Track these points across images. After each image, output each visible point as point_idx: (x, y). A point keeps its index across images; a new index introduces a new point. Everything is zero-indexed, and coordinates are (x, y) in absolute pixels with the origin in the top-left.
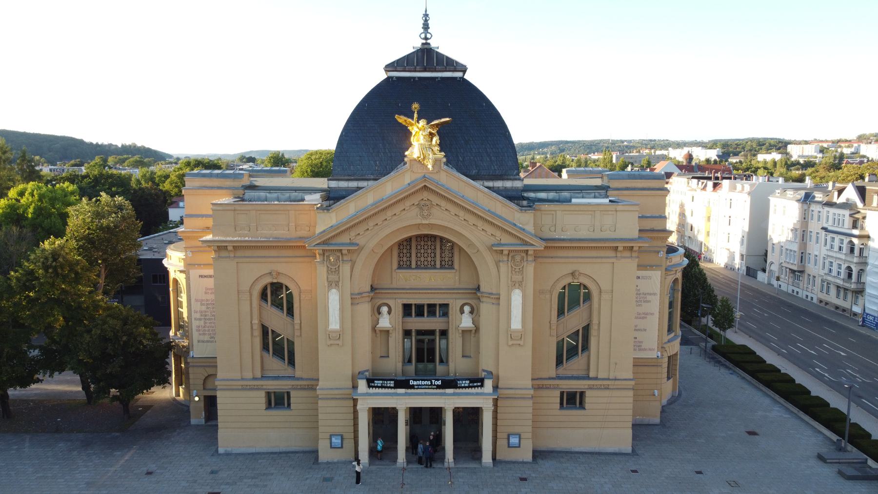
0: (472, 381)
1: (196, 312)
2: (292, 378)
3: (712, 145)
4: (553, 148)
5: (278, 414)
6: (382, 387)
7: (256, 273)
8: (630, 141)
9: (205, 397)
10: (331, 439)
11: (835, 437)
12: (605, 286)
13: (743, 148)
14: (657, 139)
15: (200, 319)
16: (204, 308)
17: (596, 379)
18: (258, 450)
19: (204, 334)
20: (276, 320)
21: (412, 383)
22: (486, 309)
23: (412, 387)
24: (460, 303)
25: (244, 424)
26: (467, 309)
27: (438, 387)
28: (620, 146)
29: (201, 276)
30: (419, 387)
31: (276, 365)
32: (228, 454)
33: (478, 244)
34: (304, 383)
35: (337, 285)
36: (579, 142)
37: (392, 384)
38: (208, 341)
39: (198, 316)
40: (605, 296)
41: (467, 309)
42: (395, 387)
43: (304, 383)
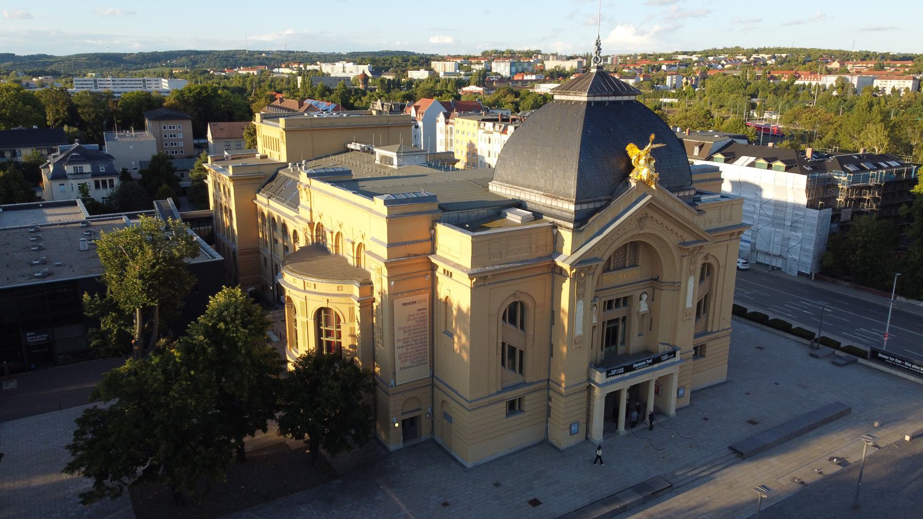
0: (669, 354)
1: (399, 340)
2: (524, 384)
3: (356, 58)
4: (184, 59)
5: (516, 418)
6: (616, 374)
7: (502, 297)
8: (267, 53)
9: (403, 421)
10: (570, 428)
11: (809, 343)
12: (722, 263)
13: (391, 63)
14: (295, 50)
15: (402, 347)
16: (406, 335)
17: (719, 331)
18: (499, 455)
19: (406, 361)
20: (514, 337)
21: (635, 366)
22: (665, 296)
23: (635, 369)
24: (638, 293)
25: (480, 434)
26: (645, 297)
27: (650, 364)
28: (259, 58)
29: (404, 304)
30: (639, 368)
31: (513, 377)
32: (477, 467)
33: (669, 243)
34: (536, 386)
35: (583, 297)
36: (211, 52)
37: (622, 370)
38: (409, 367)
39: (401, 344)
40: (721, 270)
41: (645, 297)
42: (625, 372)
43: (536, 386)
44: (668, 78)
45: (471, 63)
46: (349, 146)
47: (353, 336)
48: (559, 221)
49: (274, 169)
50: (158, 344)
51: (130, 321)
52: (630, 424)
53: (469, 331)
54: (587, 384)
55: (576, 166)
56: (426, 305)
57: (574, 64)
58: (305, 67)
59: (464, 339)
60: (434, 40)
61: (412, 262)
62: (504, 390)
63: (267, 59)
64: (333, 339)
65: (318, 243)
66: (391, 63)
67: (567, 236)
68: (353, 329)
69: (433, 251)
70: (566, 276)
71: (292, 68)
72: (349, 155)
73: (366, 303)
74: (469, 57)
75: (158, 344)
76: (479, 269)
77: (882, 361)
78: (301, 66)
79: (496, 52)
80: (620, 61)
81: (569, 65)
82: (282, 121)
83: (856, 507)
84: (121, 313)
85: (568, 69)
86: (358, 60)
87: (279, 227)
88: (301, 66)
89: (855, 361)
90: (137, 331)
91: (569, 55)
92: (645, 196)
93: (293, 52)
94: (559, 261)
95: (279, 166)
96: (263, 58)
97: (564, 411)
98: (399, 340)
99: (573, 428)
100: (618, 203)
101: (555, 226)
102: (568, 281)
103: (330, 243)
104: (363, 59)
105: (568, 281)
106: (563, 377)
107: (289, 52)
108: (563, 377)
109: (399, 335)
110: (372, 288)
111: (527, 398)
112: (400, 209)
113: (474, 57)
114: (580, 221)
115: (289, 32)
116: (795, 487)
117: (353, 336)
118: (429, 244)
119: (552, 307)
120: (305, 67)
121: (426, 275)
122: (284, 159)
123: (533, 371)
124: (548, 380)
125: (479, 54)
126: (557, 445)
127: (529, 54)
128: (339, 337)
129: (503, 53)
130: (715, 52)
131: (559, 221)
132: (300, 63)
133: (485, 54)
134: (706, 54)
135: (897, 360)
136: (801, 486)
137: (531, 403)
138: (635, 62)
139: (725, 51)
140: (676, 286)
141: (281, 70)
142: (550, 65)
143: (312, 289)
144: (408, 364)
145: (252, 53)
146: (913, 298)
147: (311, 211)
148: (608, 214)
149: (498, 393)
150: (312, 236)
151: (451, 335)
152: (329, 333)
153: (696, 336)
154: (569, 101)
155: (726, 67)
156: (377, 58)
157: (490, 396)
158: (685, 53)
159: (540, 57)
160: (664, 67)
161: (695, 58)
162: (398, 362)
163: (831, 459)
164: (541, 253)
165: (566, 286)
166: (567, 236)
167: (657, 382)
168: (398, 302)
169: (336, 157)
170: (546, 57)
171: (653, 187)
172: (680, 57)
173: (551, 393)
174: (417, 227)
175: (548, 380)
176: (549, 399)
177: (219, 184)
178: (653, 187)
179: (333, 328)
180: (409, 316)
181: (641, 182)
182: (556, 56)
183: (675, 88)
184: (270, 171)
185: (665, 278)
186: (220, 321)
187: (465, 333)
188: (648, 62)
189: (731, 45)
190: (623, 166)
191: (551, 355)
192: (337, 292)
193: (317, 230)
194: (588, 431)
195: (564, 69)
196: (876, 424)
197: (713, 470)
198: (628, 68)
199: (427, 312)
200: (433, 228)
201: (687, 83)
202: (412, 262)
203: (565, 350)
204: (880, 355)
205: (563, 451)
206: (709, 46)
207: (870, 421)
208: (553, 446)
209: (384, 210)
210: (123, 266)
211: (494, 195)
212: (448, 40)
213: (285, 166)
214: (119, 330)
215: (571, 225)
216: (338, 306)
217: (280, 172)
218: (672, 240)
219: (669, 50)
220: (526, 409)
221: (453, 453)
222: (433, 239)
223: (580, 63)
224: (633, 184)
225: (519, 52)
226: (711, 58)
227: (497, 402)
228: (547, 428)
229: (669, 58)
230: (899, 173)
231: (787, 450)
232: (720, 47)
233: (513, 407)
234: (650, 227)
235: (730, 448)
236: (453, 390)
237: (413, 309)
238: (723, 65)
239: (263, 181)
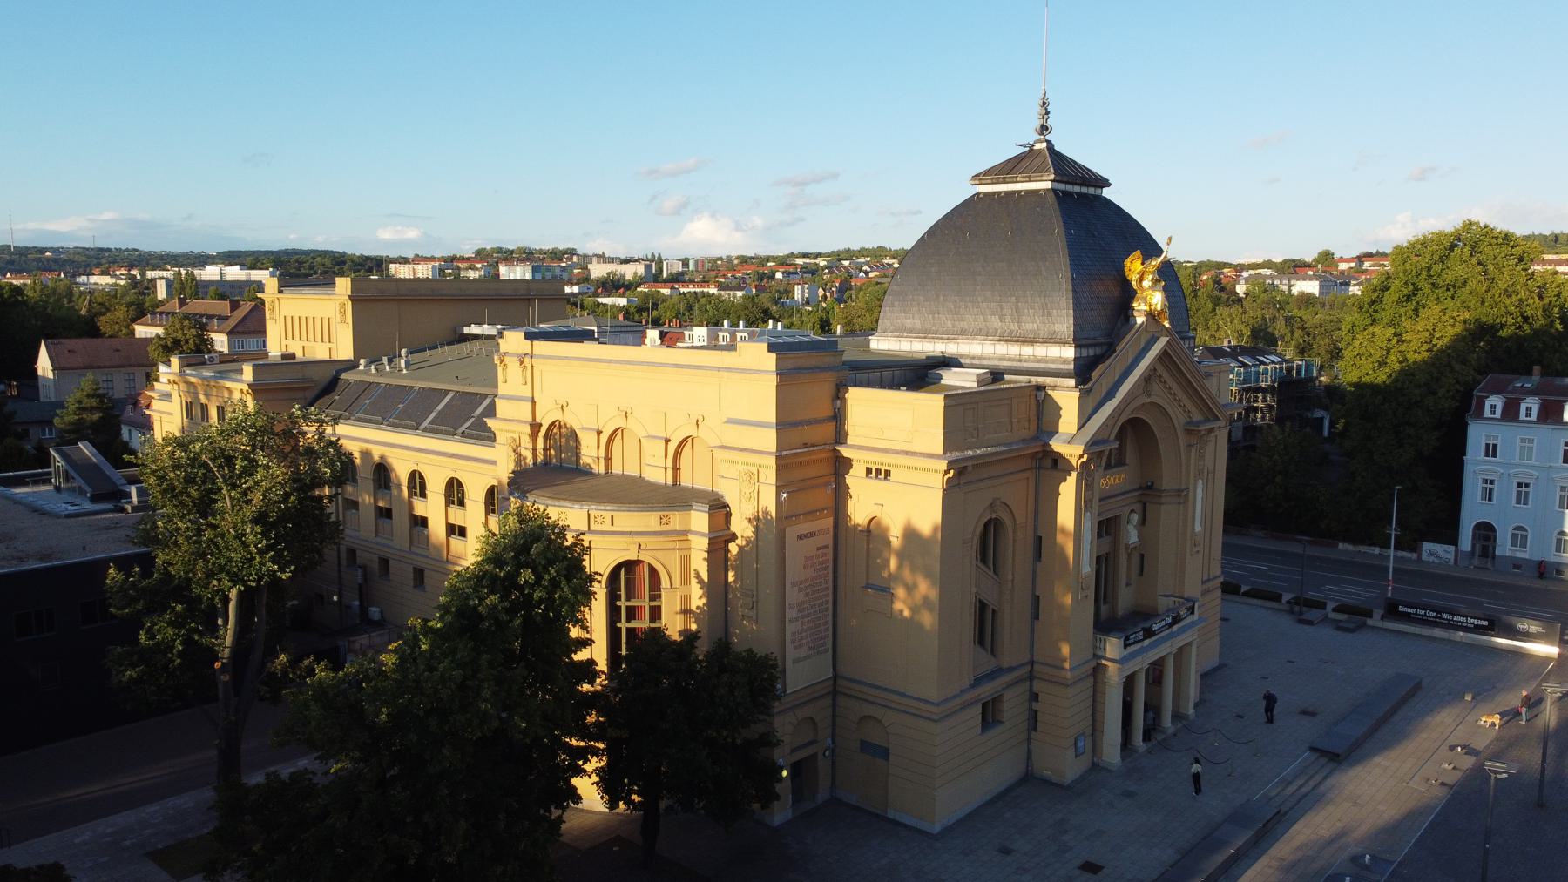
8: (54, 250)
15: (796, 619)
22: (1166, 513)
24: (1127, 510)
25: (947, 771)
27: (1171, 625)
29: (800, 537)
34: (1016, 674)
38: (805, 658)
43: (1016, 674)
44: (798, 289)
45: (459, 269)
46: (466, 330)
47: (686, 612)
48: (1041, 380)
49: (331, 373)
50: (271, 668)
51: (210, 617)
52: (1147, 736)
53: (937, 567)
54: (1093, 664)
55: (1066, 285)
56: (828, 539)
57: (640, 269)
58: (143, 274)
59: (924, 587)
60: (386, 234)
61: (813, 458)
62: (978, 682)
63: (56, 261)
64: (643, 624)
65: (546, 463)
66: (311, 267)
67: (1067, 399)
68: (686, 598)
69: (840, 437)
70: (1068, 469)
71: (115, 276)
72: (466, 347)
73: (720, 540)
74: (453, 259)
75: (271, 668)
76: (957, 455)
77: (1406, 617)
78: (134, 272)
79: (499, 250)
80: (707, 266)
81: (630, 272)
82: (343, 285)
83: (1540, 805)
84: (192, 603)
85: (629, 277)
86: (248, 260)
87: (365, 474)
88: (134, 272)
89: (1364, 625)
90: (228, 641)
91: (623, 257)
92: (1154, 340)
93: (109, 250)
94: (1057, 445)
95: (338, 367)
96: (48, 259)
97: (1064, 710)
98: (791, 607)
99: (1080, 744)
100: (1126, 347)
101: (1040, 388)
102: (1072, 480)
103: (590, 453)
104: (257, 260)
105: (1072, 480)
106: (1065, 650)
107: (101, 250)
108: (1065, 650)
109: (793, 596)
110: (729, 515)
111: (1007, 696)
112: (794, 360)
113: (463, 259)
114: (1083, 372)
115: (107, 216)
116: (1441, 793)
117: (686, 612)
118: (830, 428)
119: (1036, 528)
120: (143, 274)
121: (827, 484)
122: (345, 351)
123: (1012, 651)
124: (1032, 663)
125: (469, 253)
126: (1055, 779)
127: (556, 255)
128: (656, 613)
129: (512, 252)
130: (850, 254)
131: (1041, 380)
132: (131, 267)
133: (481, 254)
134: (838, 256)
135: (1429, 613)
136: (1445, 789)
137: (1013, 708)
138: (732, 268)
139: (863, 252)
140: (1182, 495)
141: (93, 279)
142: (598, 271)
143: (607, 527)
144: (803, 652)
145: (23, 252)
146: (1362, 543)
147: (534, 403)
148: (1114, 364)
149: (973, 686)
150: (535, 450)
151: (886, 591)
152: (632, 613)
153: (1203, 582)
154: (1013, 192)
155: (872, 275)
156: (284, 259)
157: (963, 692)
158: (805, 255)
159: (575, 259)
160: (779, 275)
161: (822, 262)
162: (789, 648)
163: (1452, 748)
164: (1025, 434)
165: (1068, 492)
166: (1067, 399)
167: (1176, 656)
168: (792, 532)
169: (456, 347)
170: (587, 259)
171: (1167, 324)
172: (800, 261)
173: (1038, 686)
174: (818, 393)
175: (1032, 663)
176: (1035, 697)
177: (204, 408)
178: (1167, 324)
179: (644, 603)
180: (807, 559)
181: (1151, 315)
182: (603, 258)
183: (808, 303)
184: (326, 375)
185: (1167, 483)
186: (521, 566)
187: (928, 575)
188: (754, 267)
189: (871, 244)
190: (1115, 292)
191: (1036, 616)
192: (658, 528)
193: (546, 437)
194: (1096, 749)
195: (623, 276)
196: (1468, 698)
197: (1312, 783)
198: (724, 276)
199: (830, 551)
200: (839, 394)
201: (825, 297)
202: (813, 458)
203: (1068, 600)
204: (1401, 609)
205: (1068, 788)
206: (839, 246)
207: (1459, 696)
208: (1047, 782)
209: (770, 361)
210: (205, 506)
211: (878, 353)
212: (412, 234)
213: (351, 365)
214: (188, 642)
215: (1072, 382)
216: (659, 555)
217: (344, 376)
218: (1179, 418)
219: (782, 251)
220: (1005, 716)
221: (891, 814)
222: (838, 417)
223: (648, 268)
224: (1140, 320)
225: (540, 251)
226: (846, 263)
227: (964, 707)
228: (1029, 752)
229: (783, 262)
230: (1289, 370)
231: (1400, 737)
232: (855, 247)
233: (990, 714)
234: (1158, 396)
235: (1313, 749)
236: (885, 690)
237: (810, 545)
238: (867, 273)
239: (310, 395)
